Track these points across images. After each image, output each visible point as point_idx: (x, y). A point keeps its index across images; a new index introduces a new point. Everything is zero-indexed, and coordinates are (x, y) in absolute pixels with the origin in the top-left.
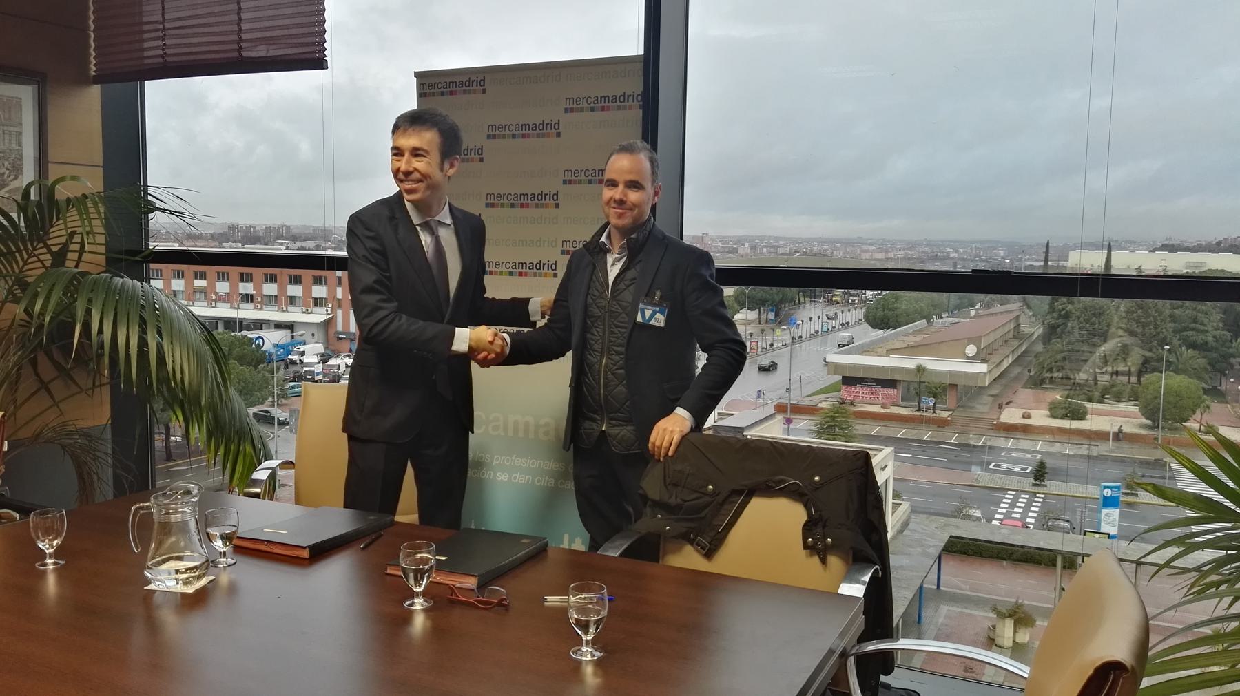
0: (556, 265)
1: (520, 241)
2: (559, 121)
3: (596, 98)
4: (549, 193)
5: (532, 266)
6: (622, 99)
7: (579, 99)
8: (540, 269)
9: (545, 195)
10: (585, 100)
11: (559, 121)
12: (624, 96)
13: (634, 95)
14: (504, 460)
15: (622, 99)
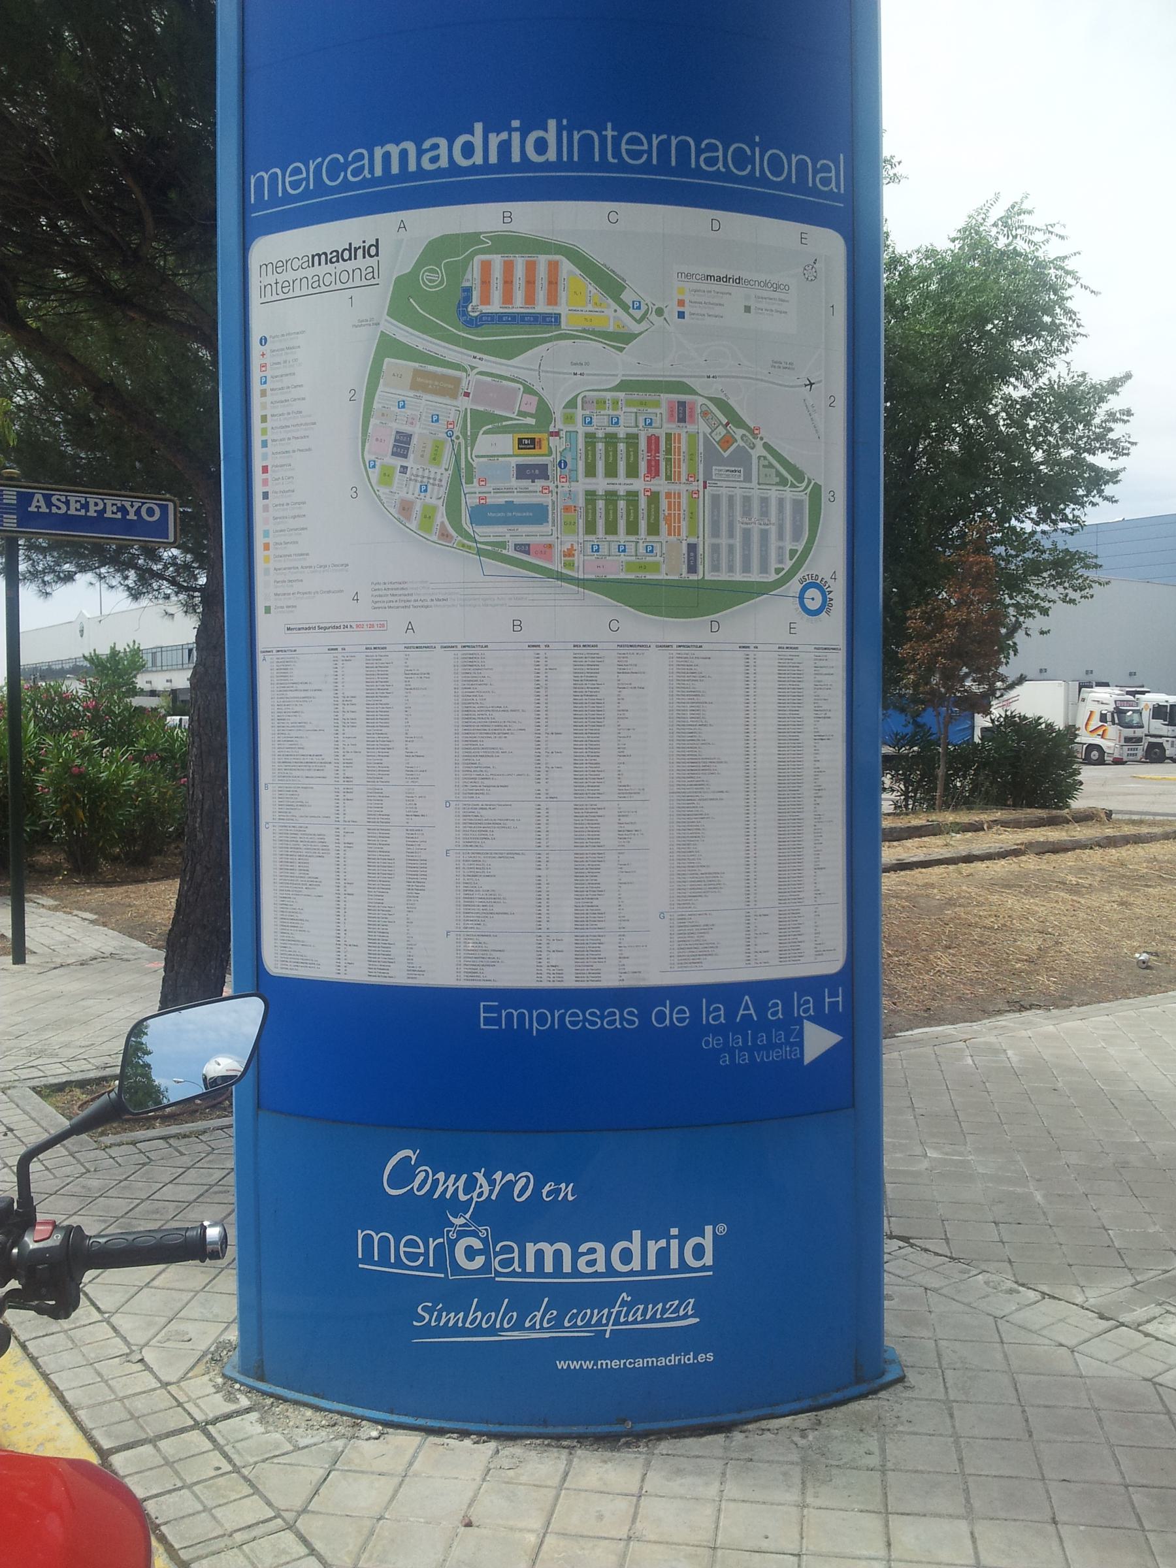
0: (377, 246)
2: (377, 240)
3: (335, 254)
4: (362, 245)
7: (281, 264)
11: (377, 240)
12: (350, 250)
13: (364, 247)
14: (318, 168)
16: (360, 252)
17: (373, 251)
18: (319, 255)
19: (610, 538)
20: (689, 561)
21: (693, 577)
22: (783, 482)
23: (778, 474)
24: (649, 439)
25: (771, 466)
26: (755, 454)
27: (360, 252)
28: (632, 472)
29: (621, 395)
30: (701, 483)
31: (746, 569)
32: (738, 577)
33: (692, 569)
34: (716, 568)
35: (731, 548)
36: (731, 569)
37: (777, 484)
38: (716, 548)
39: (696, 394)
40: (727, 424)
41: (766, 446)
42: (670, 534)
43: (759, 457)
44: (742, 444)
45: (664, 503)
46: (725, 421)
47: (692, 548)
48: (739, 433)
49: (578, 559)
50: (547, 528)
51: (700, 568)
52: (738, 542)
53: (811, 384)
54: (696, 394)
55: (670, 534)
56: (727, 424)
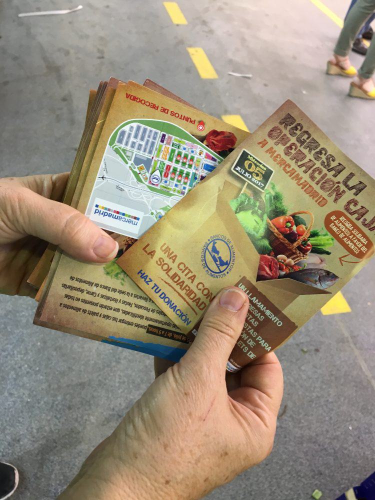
0: (95, 212)
1: (117, 219)
5: (110, 215)
6: (106, 214)
8: (105, 213)
9: (102, 214)
10: (180, 117)
15: (106, 214)
16: (101, 213)
17: (97, 211)
18: (115, 218)
19: (187, 153)
20: (164, 138)
21: (165, 133)
22: (124, 150)
23: (125, 154)
24: (167, 177)
25: (127, 156)
26: (132, 162)
27: (101, 213)
28: (177, 162)
29: (172, 192)
30: (154, 159)
31: (145, 130)
32: (149, 128)
33: (164, 136)
34: (156, 133)
35: (149, 137)
36: (151, 131)
37: (127, 150)
38: (155, 138)
39: (147, 186)
40: (139, 173)
41: (127, 163)
42: (168, 148)
43: (131, 160)
44: (136, 166)
45: (168, 157)
46: (140, 175)
47: (162, 141)
48: (137, 170)
49: (198, 151)
50: (205, 162)
51: (161, 135)
52: (146, 138)
53: (103, 178)
54: (147, 186)
55: (168, 148)
56: (139, 173)
